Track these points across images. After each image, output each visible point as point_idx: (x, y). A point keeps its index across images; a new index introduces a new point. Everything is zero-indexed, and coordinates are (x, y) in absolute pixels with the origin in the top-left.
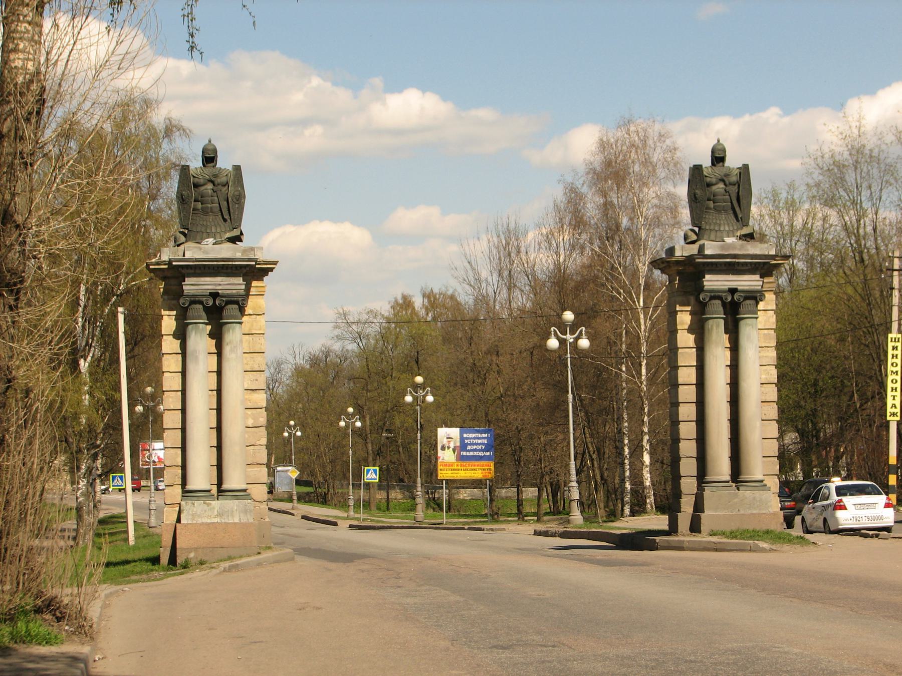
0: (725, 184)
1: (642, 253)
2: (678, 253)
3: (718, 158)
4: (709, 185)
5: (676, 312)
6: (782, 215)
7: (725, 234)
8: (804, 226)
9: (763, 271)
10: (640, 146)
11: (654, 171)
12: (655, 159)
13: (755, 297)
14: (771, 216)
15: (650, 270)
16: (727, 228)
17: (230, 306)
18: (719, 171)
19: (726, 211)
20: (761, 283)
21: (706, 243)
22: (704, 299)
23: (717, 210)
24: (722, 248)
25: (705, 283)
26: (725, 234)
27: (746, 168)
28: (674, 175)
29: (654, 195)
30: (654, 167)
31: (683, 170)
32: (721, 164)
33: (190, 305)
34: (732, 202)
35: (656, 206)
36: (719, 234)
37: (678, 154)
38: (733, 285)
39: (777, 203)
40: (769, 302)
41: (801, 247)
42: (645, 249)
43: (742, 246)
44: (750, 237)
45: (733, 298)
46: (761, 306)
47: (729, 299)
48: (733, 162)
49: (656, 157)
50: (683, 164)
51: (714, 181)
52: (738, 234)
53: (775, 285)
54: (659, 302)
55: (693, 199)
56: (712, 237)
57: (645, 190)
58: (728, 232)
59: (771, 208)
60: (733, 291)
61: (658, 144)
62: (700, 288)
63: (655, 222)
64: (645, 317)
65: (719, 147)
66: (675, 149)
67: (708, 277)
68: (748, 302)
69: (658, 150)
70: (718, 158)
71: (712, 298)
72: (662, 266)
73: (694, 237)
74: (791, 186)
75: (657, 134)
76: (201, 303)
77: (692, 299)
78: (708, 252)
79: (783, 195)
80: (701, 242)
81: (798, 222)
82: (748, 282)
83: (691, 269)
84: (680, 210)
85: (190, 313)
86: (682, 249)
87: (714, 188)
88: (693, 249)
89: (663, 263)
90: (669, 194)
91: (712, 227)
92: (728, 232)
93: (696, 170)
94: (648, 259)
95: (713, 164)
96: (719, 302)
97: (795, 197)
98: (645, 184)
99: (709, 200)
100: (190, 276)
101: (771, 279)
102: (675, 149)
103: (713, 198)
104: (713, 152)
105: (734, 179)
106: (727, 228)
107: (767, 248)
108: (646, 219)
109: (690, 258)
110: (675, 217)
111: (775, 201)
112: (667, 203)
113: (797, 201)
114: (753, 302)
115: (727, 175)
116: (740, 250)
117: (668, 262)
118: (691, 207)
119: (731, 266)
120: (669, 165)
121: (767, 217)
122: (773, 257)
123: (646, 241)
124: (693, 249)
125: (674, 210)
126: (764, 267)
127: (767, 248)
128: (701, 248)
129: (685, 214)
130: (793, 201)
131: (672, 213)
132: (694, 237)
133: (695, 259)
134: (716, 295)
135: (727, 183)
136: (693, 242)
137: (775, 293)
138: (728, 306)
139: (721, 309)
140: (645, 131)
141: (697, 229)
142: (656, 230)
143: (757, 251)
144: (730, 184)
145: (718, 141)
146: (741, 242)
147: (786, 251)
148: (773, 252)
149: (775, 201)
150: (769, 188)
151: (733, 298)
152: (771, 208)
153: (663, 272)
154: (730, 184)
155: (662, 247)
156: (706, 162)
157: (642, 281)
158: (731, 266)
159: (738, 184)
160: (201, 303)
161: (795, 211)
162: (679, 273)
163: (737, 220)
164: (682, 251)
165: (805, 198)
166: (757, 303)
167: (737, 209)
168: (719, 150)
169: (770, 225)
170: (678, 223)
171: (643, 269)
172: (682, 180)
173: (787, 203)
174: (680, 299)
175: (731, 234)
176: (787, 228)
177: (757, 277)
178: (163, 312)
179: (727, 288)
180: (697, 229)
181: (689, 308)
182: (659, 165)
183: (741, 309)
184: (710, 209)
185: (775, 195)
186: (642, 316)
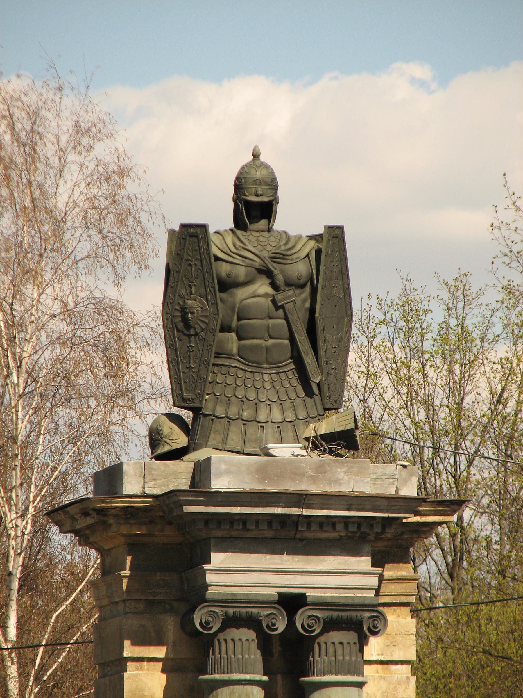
0: (274, 285)
1: (16, 481)
2: (131, 486)
3: (254, 206)
4: (226, 285)
5: (121, 664)
6: (431, 373)
7: (270, 431)
8: (495, 413)
9: (381, 545)
10: (19, 160)
11: (58, 233)
12: (61, 202)
13: (357, 621)
14: (398, 379)
15: (40, 531)
16: (277, 416)
17: (234, 633)
18: (256, 243)
19: (274, 364)
20: (374, 581)
21: (216, 456)
22: (205, 625)
23: (251, 360)
24: (262, 472)
25: (210, 578)
26: (270, 431)
27: (335, 235)
28: (116, 248)
29: (57, 308)
30: (59, 225)
31: (146, 235)
32: (263, 223)
33: (221, 630)
34: (292, 339)
35: (62, 340)
36: (252, 430)
37: (131, 187)
38: (293, 583)
39: (416, 338)
40: (398, 637)
41: (483, 472)
42: (27, 467)
43: (320, 469)
44: (342, 442)
45: (291, 623)
46: (374, 649)
47: (281, 626)
48: (297, 218)
49: (67, 192)
50: (144, 217)
51: (241, 272)
52: (310, 433)
53: (412, 587)
54: (68, 626)
55: (179, 323)
56: (234, 441)
57: (30, 291)
58: (279, 426)
59: (400, 354)
60: (292, 602)
61: (72, 157)
62: (195, 594)
63: (62, 386)
64: (23, 675)
65: (260, 174)
66: (122, 172)
67: (217, 559)
68: (335, 636)
69: (72, 174)
70: (254, 206)
71: (231, 622)
72: (83, 522)
73: (181, 440)
74: (459, 291)
75: (67, 125)
76: (252, 622)
77: (171, 625)
78: (219, 484)
79: (436, 316)
80: (200, 455)
81: (478, 397)
82: (336, 576)
83: (168, 535)
84: (134, 353)
85: (219, 653)
86: (144, 473)
87: (241, 293)
88: (175, 475)
89: (86, 514)
90: (104, 308)
91: (233, 411)
92: (279, 426)
93: (190, 239)
94: (32, 496)
95: (239, 223)
96: (252, 635)
97: (469, 323)
98: (31, 274)
99: (225, 329)
100: (230, 544)
101: (404, 570)
102: (122, 172)
103: (238, 323)
104: (239, 186)
105: (300, 269)
106: (277, 416)
107: (394, 476)
108: (32, 377)
109: (167, 503)
110: (117, 376)
111: (409, 335)
112: (92, 330)
113: (476, 334)
114: (349, 637)
115: (279, 257)
116: (313, 480)
117: (102, 512)
118: (171, 347)
119: (290, 528)
120: (102, 218)
121: (385, 381)
122: (411, 504)
123: (27, 444)
124: (176, 476)
125: (114, 356)
126: (384, 534)
127: (394, 476)
128: (202, 471)
129: (151, 364)
130: (465, 335)
131: (108, 361)
132: (181, 440)
133: (181, 505)
134: (240, 615)
135: (280, 279)
136: (177, 454)
137: (415, 613)
138: (276, 649)
139: (256, 656)
140: (34, 116)
141: (187, 415)
142: (61, 411)
143: (365, 486)
144: (289, 284)
145: (256, 156)
146: (316, 457)
147: (444, 485)
148: (410, 490)
149: (409, 335)
150: (395, 295)
151: (291, 623)
152: (400, 354)
153: (84, 538)
154: (289, 284)
155: (78, 462)
156: (218, 215)
157: (15, 566)
158: (290, 528)
159: (311, 284)
160: (252, 622)
161: (468, 365)
162: (134, 546)
163: (309, 393)
164: (143, 479)
165: (498, 329)
166: (362, 641)
167: (308, 358)
168: (257, 182)
169: (395, 404)
170: (128, 392)
171: (20, 527)
172: (142, 264)
173: (445, 340)
174: (133, 623)
175: (289, 433)
176: (443, 413)
177: (363, 563)
178: (129, 650)
179: (274, 591)
180: (187, 415)
181: (160, 652)
182: (74, 219)
183: (315, 659)
184: (229, 356)
185: (411, 312)
186: (13, 670)
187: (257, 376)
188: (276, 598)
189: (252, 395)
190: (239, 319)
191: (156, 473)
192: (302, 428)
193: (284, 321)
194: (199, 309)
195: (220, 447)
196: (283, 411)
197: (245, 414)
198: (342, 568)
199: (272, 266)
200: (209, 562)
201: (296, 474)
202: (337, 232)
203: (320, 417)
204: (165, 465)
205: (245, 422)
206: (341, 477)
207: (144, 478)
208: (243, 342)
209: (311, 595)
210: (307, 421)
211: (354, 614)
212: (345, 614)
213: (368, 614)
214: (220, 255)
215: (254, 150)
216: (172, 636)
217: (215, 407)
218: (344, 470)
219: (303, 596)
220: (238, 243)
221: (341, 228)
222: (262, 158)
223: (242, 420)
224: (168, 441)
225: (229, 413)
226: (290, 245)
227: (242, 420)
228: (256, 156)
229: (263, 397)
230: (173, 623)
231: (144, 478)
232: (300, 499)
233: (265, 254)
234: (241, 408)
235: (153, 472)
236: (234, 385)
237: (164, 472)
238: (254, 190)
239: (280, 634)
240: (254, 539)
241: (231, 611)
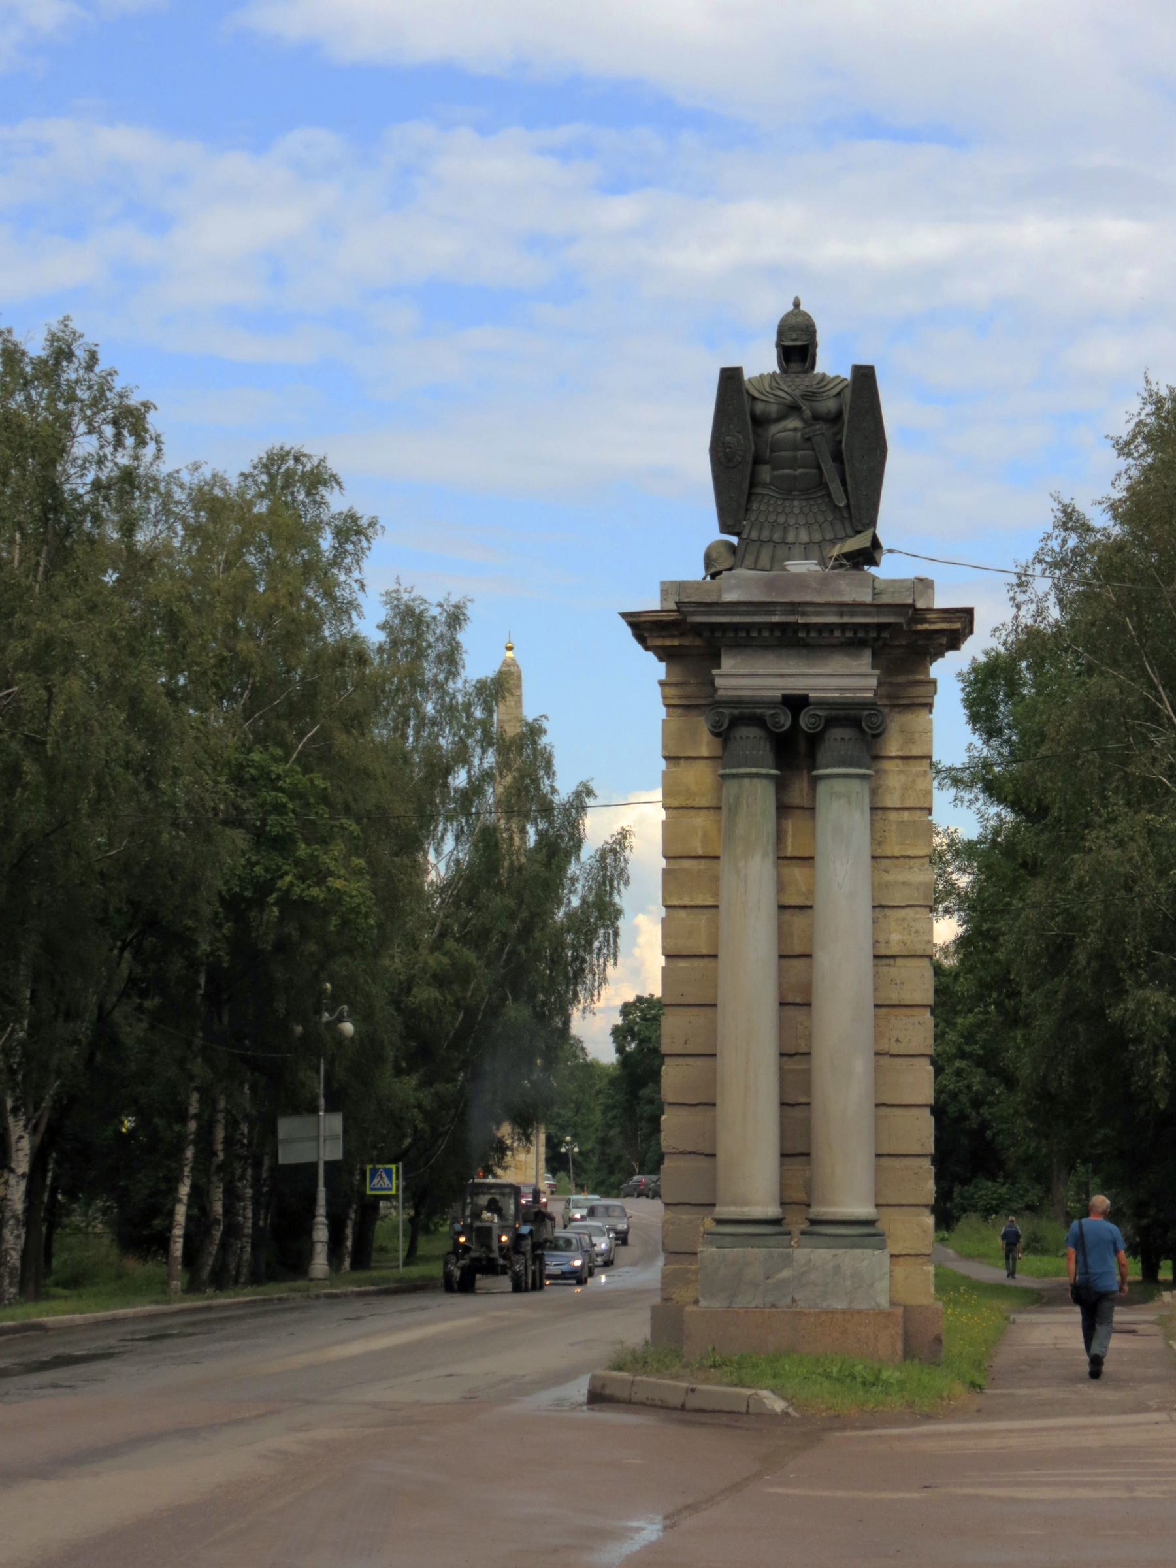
3: (797, 346)
25: (719, 682)
48: (832, 363)
51: (773, 409)
60: (796, 703)
70: (797, 346)
76: (758, 721)
87: (774, 429)
145: (797, 305)
160: (758, 721)
179: (778, 694)
187: (787, 503)
188: (780, 700)
189: (781, 519)
190: (772, 451)
196: (810, 534)
198: (846, 671)
200: (719, 667)
202: (865, 376)
203: (843, 539)
208: (775, 473)
210: (833, 542)
211: (852, 712)
212: (842, 713)
213: (866, 713)
214: (756, 394)
219: (806, 697)
221: (663, 583)
226: (824, 383)
228: (797, 305)
229: (792, 521)
232: (793, 608)
233: (798, 393)
234: (772, 532)
241: (736, 712)
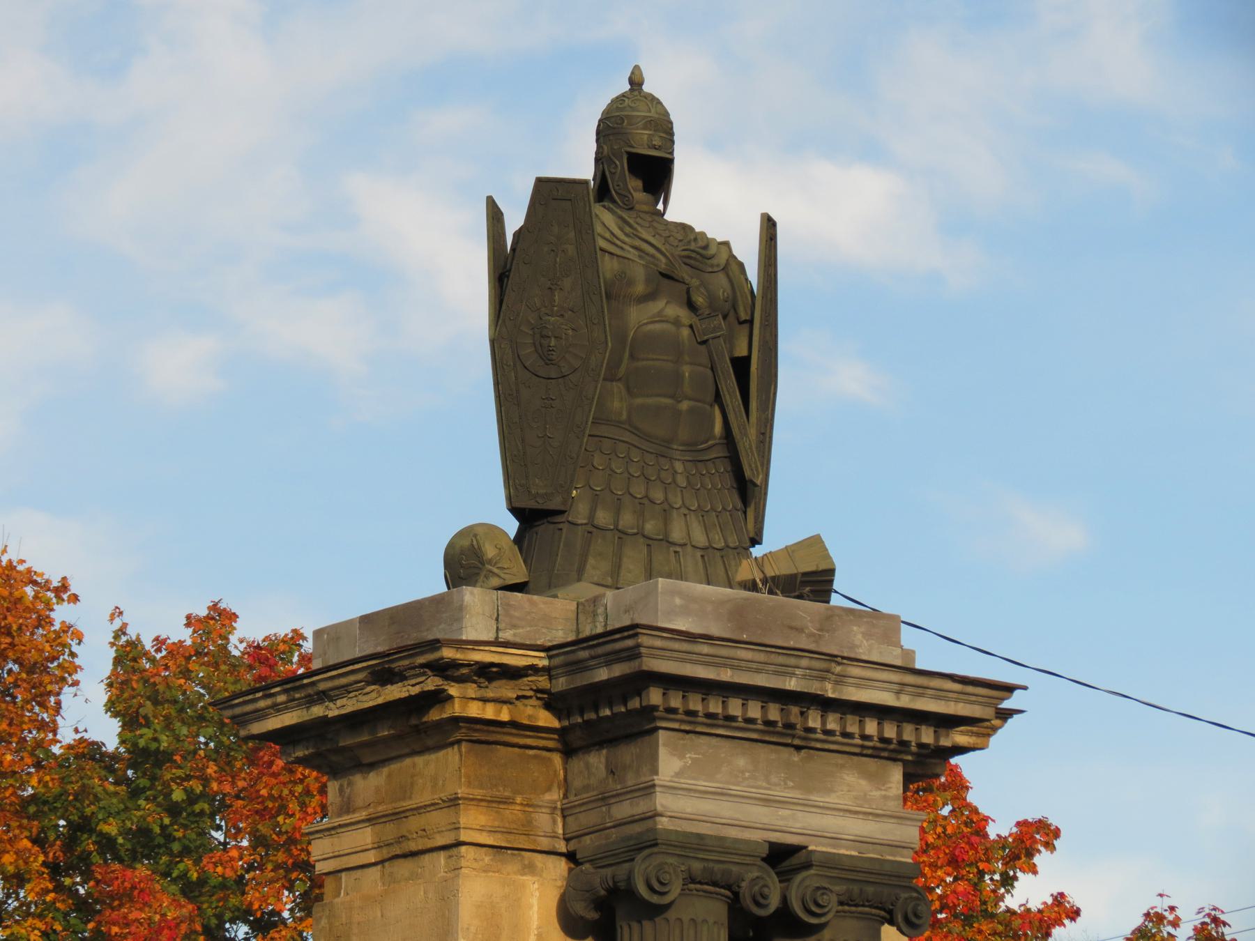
16: (700, 538)
60: (782, 856)
91: (627, 520)
106: (700, 538)
145: (636, 82)
188: (764, 851)
189: (658, 495)
191: (516, 614)
192: (733, 563)
193: (709, 372)
194: (570, 332)
195: (609, 581)
197: (649, 527)
199: (684, 273)
201: (791, 628)
204: (530, 601)
205: (650, 542)
206: (857, 642)
207: (497, 619)
209: (819, 849)
215: (632, 73)
216: (536, 916)
217: (593, 511)
218: (863, 629)
220: (628, 229)
222: (646, 88)
223: (644, 536)
224: (496, 570)
225: (621, 523)
227: (644, 536)
230: (537, 894)
231: (497, 619)
235: (512, 612)
236: (626, 475)
237: (529, 613)
238: (645, 137)
239: (760, 918)
240: (328, 829)
